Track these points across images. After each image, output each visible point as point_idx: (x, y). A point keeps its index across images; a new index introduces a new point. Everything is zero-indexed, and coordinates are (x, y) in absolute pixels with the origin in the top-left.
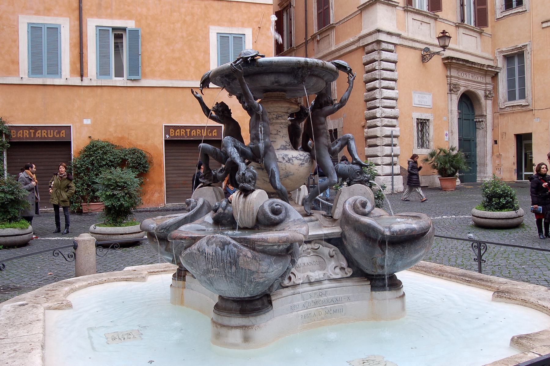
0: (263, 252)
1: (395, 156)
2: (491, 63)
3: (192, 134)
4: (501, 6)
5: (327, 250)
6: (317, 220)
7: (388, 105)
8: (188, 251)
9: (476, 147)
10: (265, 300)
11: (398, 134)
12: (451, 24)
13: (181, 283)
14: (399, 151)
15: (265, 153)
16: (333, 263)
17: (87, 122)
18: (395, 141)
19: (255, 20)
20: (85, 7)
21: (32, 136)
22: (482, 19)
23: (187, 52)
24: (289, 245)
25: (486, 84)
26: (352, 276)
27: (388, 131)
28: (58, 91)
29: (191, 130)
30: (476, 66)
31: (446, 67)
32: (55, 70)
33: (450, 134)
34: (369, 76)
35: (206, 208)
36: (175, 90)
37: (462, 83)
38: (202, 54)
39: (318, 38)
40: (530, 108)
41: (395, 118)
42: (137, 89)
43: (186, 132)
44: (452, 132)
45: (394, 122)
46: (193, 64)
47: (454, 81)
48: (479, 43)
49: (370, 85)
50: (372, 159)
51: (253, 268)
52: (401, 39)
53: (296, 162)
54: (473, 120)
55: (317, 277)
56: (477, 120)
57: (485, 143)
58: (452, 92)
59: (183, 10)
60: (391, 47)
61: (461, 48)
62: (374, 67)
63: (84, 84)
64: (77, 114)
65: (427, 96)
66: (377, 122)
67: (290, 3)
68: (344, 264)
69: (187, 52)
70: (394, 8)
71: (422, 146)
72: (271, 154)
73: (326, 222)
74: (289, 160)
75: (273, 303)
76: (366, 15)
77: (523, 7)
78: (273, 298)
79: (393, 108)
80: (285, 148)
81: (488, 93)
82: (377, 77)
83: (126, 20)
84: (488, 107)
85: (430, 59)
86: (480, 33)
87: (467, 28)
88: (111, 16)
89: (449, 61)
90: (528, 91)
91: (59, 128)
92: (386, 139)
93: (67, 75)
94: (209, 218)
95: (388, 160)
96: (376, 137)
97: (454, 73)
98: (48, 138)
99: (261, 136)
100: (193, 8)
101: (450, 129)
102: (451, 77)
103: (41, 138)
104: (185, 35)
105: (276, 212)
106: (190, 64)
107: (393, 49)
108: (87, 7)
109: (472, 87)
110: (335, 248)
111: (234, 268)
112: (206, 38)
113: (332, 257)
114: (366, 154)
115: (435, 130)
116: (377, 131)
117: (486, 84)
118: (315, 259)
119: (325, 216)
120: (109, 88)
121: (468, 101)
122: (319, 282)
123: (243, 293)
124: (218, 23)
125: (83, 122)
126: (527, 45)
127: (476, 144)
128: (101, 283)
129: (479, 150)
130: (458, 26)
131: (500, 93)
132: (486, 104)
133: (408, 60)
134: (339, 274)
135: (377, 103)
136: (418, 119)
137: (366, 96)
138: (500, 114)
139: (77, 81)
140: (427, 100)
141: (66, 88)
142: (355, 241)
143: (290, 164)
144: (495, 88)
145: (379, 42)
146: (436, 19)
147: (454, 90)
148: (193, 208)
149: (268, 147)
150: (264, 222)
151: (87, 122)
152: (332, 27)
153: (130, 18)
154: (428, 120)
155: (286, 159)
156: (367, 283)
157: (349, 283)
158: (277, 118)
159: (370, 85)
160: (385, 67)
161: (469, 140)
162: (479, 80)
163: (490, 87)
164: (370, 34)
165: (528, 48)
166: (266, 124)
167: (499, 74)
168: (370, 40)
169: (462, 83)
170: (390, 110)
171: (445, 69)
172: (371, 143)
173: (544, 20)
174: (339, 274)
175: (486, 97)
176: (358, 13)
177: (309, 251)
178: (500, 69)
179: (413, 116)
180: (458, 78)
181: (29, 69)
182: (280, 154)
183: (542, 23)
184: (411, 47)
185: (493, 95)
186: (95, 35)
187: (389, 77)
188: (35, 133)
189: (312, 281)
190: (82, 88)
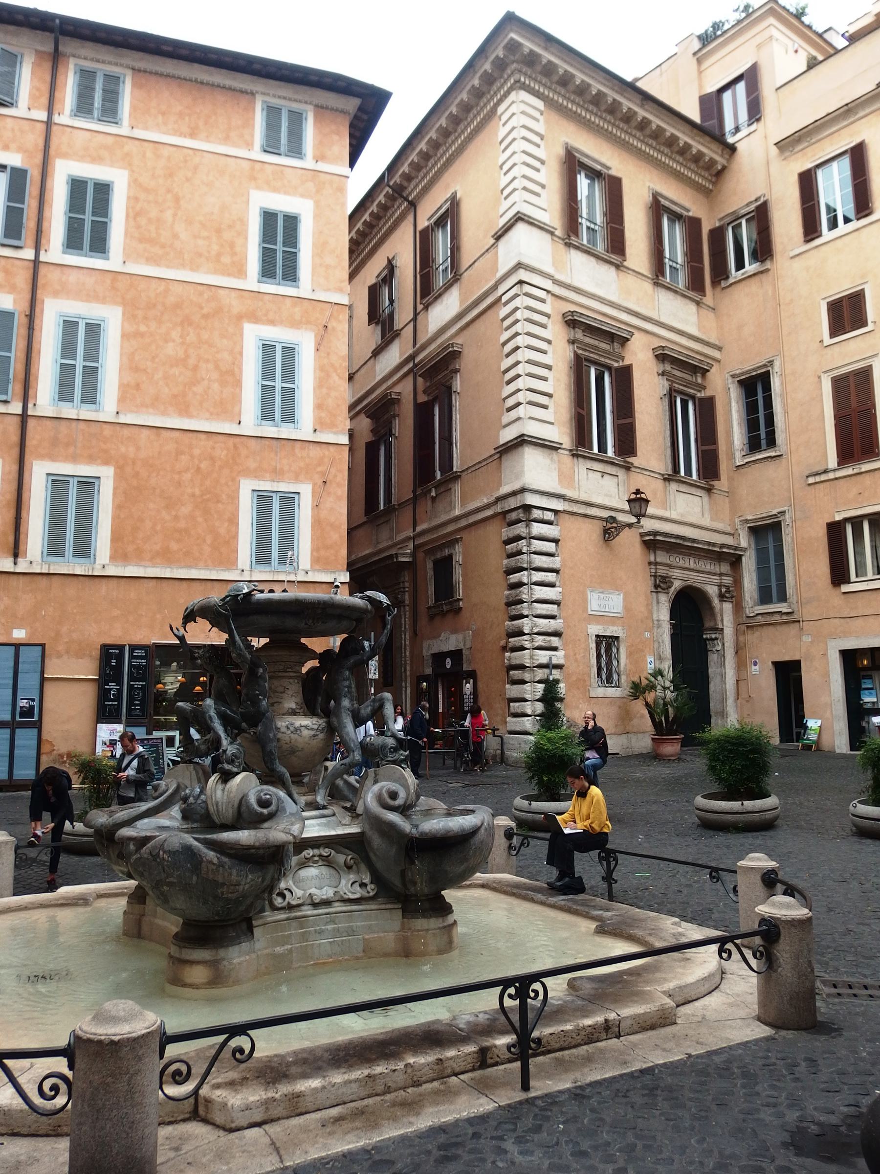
2: (729, 541)
4: (742, 446)
6: (334, 815)
7: (544, 612)
11: (561, 661)
12: (656, 476)
19: (319, 469)
20: (31, 442)
22: (710, 468)
23: (200, 519)
25: (721, 575)
27: (543, 657)
34: (512, 562)
36: (177, 583)
37: (676, 573)
38: (226, 525)
39: (433, 494)
40: (795, 617)
41: (557, 634)
45: (555, 641)
46: (209, 540)
48: (706, 507)
49: (514, 578)
50: (517, 704)
52: (567, 503)
55: (324, 897)
57: (723, 676)
59: (196, 452)
60: (549, 516)
61: (674, 516)
62: (519, 548)
63: (19, 570)
65: (614, 597)
66: (525, 641)
67: (391, 430)
69: (200, 519)
70: (554, 452)
74: (296, 729)
76: (508, 461)
77: (777, 449)
79: (553, 617)
80: (293, 713)
81: (723, 590)
82: (525, 566)
83: (98, 465)
85: (617, 535)
86: (709, 490)
87: (684, 482)
88: (74, 459)
90: (789, 591)
96: (522, 667)
100: (213, 448)
102: (656, 564)
104: (197, 492)
106: (204, 541)
107: (552, 519)
108: (34, 442)
109: (696, 580)
112: (234, 498)
114: (507, 696)
115: (630, 655)
116: (524, 657)
117: (721, 575)
118: (325, 870)
120: (62, 577)
122: (327, 903)
124: (256, 474)
125: (11, 633)
126: (785, 512)
129: (714, 686)
130: (667, 479)
131: (746, 590)
132: (721, 610)
133: (582, 537)
135: (525, 609)
137: (507, 597)
138: (748, 627)
140: (614, 603)
143: (296, 736)
144: (738, 582)
145: (527, 508)
146: (628, 469)
148: (162, 795)
150: (244, 817)
152: (457, 477)
153: (106, 463)
154: (617, 638)
155: (292, 728)
156: (396, 906)
159: (514, 578)
160: (538, 549)
162: (708, 567)
163: (727, 580)
164: (514, 494)
165: (787, 516)
167: (743, 558)
168: (513, 503)
169: (676, 573)
170: (547, 620)
171: (647, 551)
172: (516, 678)
173: (807, 473)
174: (358, 892)
175: (722, 597)
176: (496, 457)
177: (316, 858)
178: (745, 550)
179: (589, 631)
180: (670, 566)
183: (807, 477)
184: (585, 516)
185: (734, 594)
186: (44, 489)
187: (545, 566)
190: (15, 577)
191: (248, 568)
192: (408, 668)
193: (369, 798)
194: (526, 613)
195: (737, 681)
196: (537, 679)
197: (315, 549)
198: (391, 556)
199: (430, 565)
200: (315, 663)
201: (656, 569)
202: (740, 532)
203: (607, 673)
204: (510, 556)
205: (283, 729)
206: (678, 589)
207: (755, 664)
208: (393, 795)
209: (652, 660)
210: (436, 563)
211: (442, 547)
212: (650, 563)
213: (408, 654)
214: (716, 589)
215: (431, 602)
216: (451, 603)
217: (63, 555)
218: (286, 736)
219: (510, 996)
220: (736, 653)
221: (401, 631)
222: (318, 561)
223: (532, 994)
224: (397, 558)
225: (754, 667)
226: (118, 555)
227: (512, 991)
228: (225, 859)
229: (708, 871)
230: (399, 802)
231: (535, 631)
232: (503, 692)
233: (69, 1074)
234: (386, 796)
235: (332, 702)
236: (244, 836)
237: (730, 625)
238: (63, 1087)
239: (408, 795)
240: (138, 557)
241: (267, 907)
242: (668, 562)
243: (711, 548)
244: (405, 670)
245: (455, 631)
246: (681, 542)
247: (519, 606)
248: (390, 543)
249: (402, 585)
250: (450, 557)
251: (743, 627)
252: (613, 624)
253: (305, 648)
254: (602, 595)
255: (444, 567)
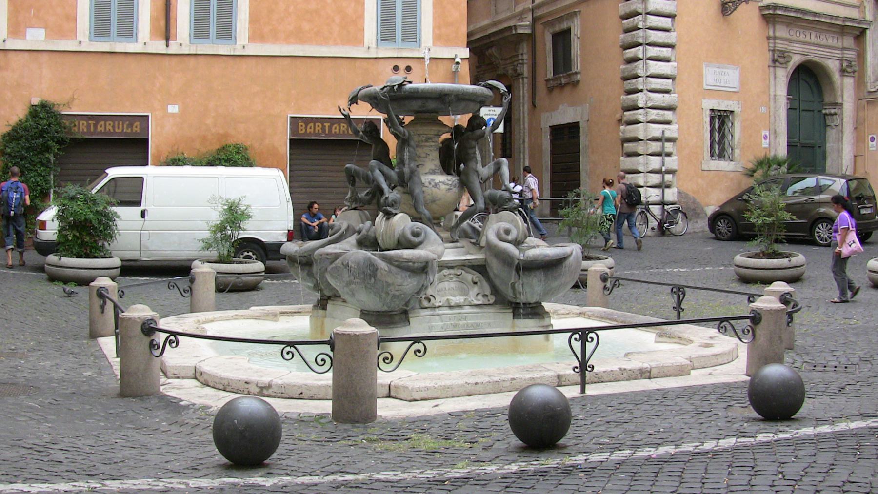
0: (398, 267)
1: (668, 172)
2: (854, 14)
3: (333, 131)
5: (470, 276)
7: (658, 87)
8: (333, 265)
9: (824, 158)
10: (403, 316)
11: (675, 135)
13: (321, 312)
14: (676, 163)
15: (411, 178)
16: (476, 289)
17: (173, 109)
18: (669, 147)
21: (92, 130)
24: (424, 264)
25: (843, 49)
26: (495, 303)
27: (656, 130)
28: (132, 62)
29: (332, 125)
30: (823, 20)
31: (768, 22)
32: (128, 30)
33: (772, 136)
34: (629, 38)
35: (349, 231)
36: (308, 60)
37: (796, 47)
42: (249, 58)
43: (323, 128)
44: (775, 132)
46: (337, 19)
47: (781, 45)
49: (630, 53)
51: (390, 280)
53: (443, 187)
54: (820, 111)
56: (827, 111)
57: (840, 151)
58: (777, 64)
62: (635, 23)
64: (159, 97)
65: (730, 72)
66: (640, 115)
68: (488, 291)
71: (721, 156)
72: (415, 178)
73: (473, 249)
75: (411, 320)
78: (411, 315)
79: (667, 92)
80: (433, 172)
81: (845, 64)
82: (641, 41)
84: (846, 91)
85: (735, 9)
89: (771, 12)
91: (131, 119)
92: (654, 144)
93: (145, 38)
94: (353, 239)
95: (655, 179)
96: (637, 140)
97: (781, 31)
98: (115, 133)
99: (407, 162)
101: (772, 128)
102: (775, 38)
103: (105, 133)
105: (416, 234)
106: (333, 21)
109: (816, 55)
110: (479, 275)
111: (373, 280)
113: (475, 283)
115: (744, 128)
116: (639, 131)
117: (843, 49)
119: (474, 244)
121: (808, 79)
122: (459, 306)
123: (381, 304)
127: (824, 153)
128: (227, 319)
132: (842, 84)
134: (481, 300)
135: (639, 83)
136: (712, 110)
137: (623, 71)
139: (159, 46)
140: (731, 78)
141: (143, 57)
142: (495, 267)
147: (780, 60)
149: (412, 172)
151: (173, 109)
154: (732, 112)
155: (433, 184)
157: (491, 310)
158: (426, 141)
159: (630, 53)
160: (654, 24)
161: (812, 147)
162: (830, 42)
163: (851, 55)
166: (411, 149)
167: (868, 32)
170: (661, 95)
174: (481, 300)
175: (843, 72)
180: (790, 41)
181: (90, 28)
182: (425, 179)
185: (857, 69)
187: (661, 41)
188: (95, 126)
189: (452, 304)
190: (167, 58)
191: (374, 46)
192: (527, 140)
193: (491, 234)
194: (641, 87)
195: (855, 156)
196: (650, 152)
197: (437, 26)
198: (510, 28)
199: (549, 38)
200: (447, 136)
201: (775, 43)
202: (866, 4)
203: (720, 147)
204: (627, 31)
205: (427, 184)
206: (797, 64)
207: (872, 139)
208: (507, 232)
209: (768, 134)
210: (556, 36)
211: (561, 19)
212: (768, 38)
213: (526, 125)
214: (837, 63)
215: (550, 75)
216: (569, 76)
217: (208, 37)
218: (430, 191)
219: (576, 339)
220: (856, 128)
221: (519, 104)
222: (439, 39)
223: (590, 340)
224: (516, 29)
225: (870, 143)
226: (256, 36)
227: (577, 336)
228: (393, 268)
229: (747, 297)
230: (510, 238)
231: (649, 105)
232: (617, 162)
233: (331, 354)
234: (502, 232)
235: (462, 165)
236: (406, 253)
237: (850, 100)
238: (328, 360)
239: (518, 233)
240: (275, 37)
241: (417, 306)
242: (788, 36)
243: (833, 22)
244: (524, 142)
245: (572, 104)
246: (799, 15)
247: (634, 81)
248: (509, 14)
249: (520, 57)
250: (568, 31)
251: (864, 102)
252: (729, 99)
253: (441, 124)
254: (718, 70)
255: (562, 39)
